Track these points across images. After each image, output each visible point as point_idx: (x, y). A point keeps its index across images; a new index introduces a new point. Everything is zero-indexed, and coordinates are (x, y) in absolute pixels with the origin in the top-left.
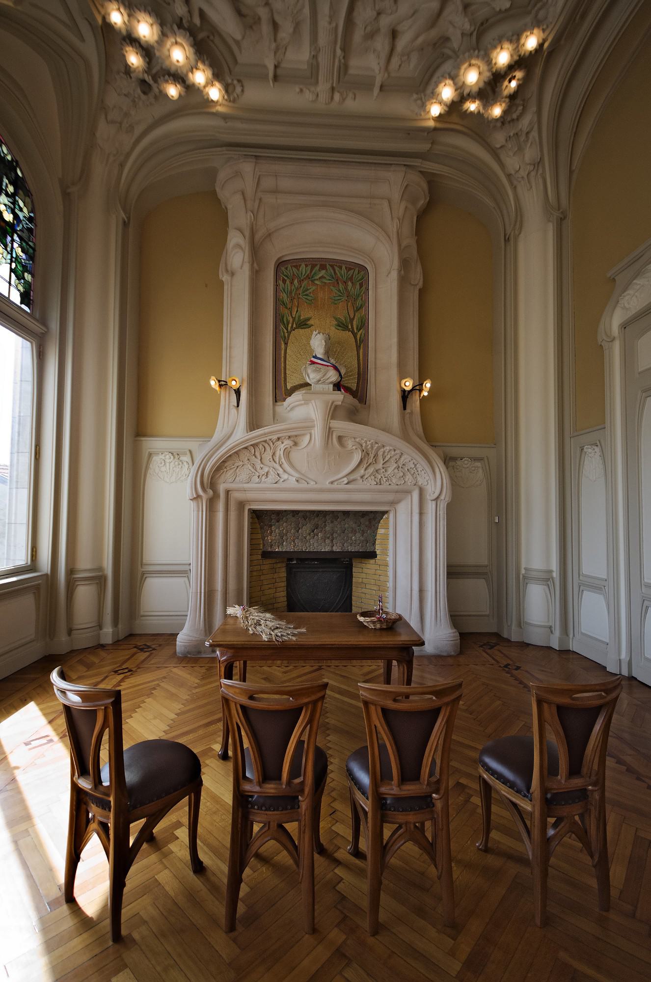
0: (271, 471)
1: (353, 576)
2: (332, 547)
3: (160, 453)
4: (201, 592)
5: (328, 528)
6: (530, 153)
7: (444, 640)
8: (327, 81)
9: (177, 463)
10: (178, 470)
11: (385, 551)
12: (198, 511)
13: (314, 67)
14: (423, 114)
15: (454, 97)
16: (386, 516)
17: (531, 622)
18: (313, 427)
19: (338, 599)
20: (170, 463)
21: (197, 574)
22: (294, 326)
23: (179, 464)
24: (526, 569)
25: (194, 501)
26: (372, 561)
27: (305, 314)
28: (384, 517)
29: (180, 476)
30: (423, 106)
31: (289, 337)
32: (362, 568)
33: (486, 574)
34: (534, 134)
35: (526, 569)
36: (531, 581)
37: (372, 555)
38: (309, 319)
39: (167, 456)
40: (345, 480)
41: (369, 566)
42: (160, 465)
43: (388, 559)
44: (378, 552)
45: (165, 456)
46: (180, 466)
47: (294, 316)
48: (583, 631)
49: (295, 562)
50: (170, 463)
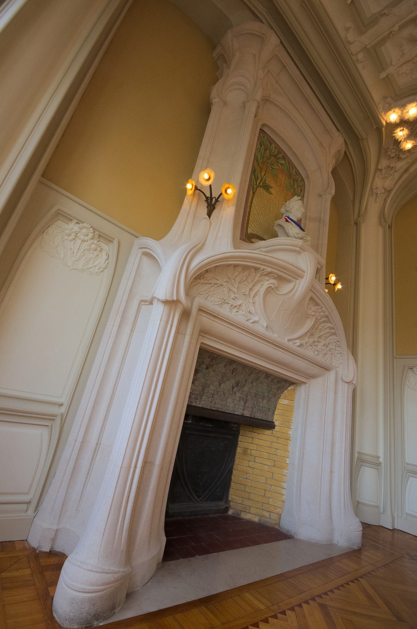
0: (244, 305)
1: (238, 446)
2: (244, 410)
3: (76, 221)
4: (136, 467)
5: (246, 389)
6: (388, 183)
7: (356, 530)
8: (370, 38)
9: (93, 246)
10: (91, 256)
11: (287, 423)
12: (167, 322)
13: (374, 21)
14: (383, 113)
15: (397, 119)
16: (292, 387)
17: (363, 501)
18: (302, 277)
19: (184, 468)
20: (83, 241)
21: (138, 433)
22: (261, 184)
23: (96, 250)
24: (359, 453)
25: (166, 307)
26: (268, 432)
27: (270, 181)
28: (289, 388)
29: (91, 266)
30: (389, 108)
31: (256, 189)
32: (253, 438)
33: (51, 418)
34: (397, 176)
35: (359, 453)
36: (364, 464)
37: (270, 425)
38: (271, 188)
39: (84, 231)
40: (298, 342)
41: (261, 436)
42: (66, 237)
43: (290, 432)
44: (276, 423)
45: (81, 229)
46: (96, 253)
47: (262, 176)
48: (407, 511)
49: (190, 422)
50: (83, 241)
